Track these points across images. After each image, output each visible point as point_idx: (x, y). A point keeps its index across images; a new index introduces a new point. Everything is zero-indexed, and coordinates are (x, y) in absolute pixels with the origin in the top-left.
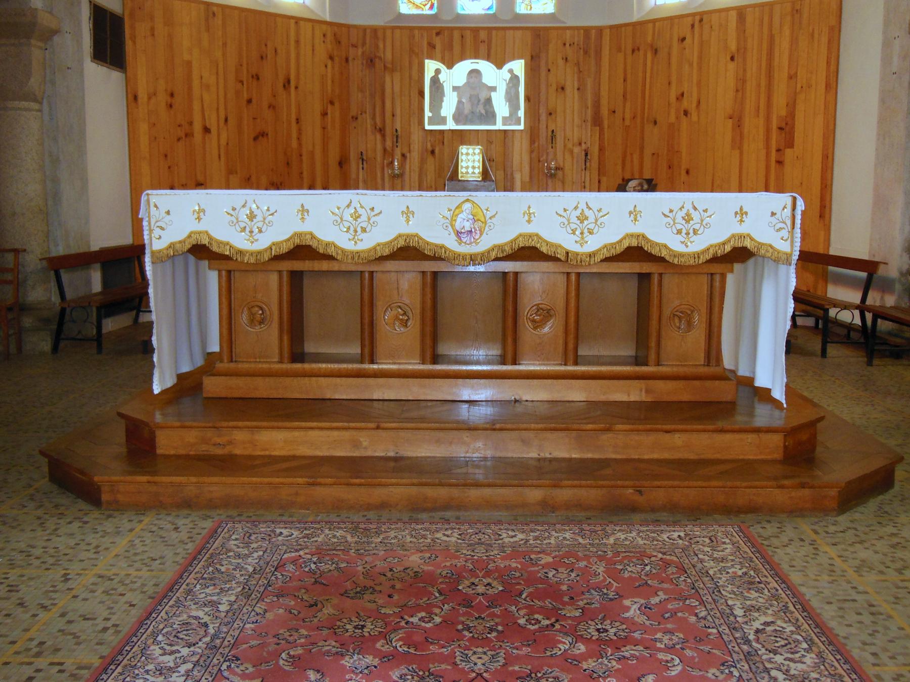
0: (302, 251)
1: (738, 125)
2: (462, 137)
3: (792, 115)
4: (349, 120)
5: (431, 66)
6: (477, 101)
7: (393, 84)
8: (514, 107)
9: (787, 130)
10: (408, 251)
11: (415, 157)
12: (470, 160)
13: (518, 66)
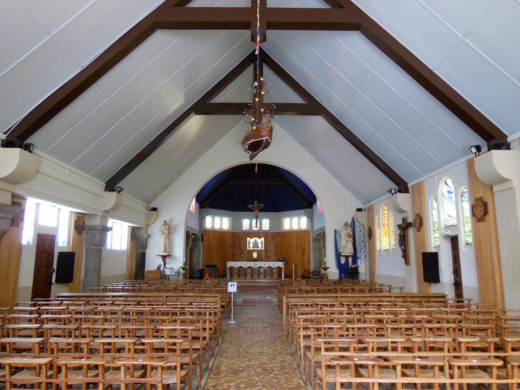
0: (241, 267)
1: (297, 249)
2: (254, 251)
3: (304, 248)
4: (234, 247)
5: (248, 239)
6: (256, 244)
7: (242, 242)
8: (262, 246)
9: (304, 250)
10: (250, 267)
11: (245, 254)
12: (255, 255)
13: (263, 239)
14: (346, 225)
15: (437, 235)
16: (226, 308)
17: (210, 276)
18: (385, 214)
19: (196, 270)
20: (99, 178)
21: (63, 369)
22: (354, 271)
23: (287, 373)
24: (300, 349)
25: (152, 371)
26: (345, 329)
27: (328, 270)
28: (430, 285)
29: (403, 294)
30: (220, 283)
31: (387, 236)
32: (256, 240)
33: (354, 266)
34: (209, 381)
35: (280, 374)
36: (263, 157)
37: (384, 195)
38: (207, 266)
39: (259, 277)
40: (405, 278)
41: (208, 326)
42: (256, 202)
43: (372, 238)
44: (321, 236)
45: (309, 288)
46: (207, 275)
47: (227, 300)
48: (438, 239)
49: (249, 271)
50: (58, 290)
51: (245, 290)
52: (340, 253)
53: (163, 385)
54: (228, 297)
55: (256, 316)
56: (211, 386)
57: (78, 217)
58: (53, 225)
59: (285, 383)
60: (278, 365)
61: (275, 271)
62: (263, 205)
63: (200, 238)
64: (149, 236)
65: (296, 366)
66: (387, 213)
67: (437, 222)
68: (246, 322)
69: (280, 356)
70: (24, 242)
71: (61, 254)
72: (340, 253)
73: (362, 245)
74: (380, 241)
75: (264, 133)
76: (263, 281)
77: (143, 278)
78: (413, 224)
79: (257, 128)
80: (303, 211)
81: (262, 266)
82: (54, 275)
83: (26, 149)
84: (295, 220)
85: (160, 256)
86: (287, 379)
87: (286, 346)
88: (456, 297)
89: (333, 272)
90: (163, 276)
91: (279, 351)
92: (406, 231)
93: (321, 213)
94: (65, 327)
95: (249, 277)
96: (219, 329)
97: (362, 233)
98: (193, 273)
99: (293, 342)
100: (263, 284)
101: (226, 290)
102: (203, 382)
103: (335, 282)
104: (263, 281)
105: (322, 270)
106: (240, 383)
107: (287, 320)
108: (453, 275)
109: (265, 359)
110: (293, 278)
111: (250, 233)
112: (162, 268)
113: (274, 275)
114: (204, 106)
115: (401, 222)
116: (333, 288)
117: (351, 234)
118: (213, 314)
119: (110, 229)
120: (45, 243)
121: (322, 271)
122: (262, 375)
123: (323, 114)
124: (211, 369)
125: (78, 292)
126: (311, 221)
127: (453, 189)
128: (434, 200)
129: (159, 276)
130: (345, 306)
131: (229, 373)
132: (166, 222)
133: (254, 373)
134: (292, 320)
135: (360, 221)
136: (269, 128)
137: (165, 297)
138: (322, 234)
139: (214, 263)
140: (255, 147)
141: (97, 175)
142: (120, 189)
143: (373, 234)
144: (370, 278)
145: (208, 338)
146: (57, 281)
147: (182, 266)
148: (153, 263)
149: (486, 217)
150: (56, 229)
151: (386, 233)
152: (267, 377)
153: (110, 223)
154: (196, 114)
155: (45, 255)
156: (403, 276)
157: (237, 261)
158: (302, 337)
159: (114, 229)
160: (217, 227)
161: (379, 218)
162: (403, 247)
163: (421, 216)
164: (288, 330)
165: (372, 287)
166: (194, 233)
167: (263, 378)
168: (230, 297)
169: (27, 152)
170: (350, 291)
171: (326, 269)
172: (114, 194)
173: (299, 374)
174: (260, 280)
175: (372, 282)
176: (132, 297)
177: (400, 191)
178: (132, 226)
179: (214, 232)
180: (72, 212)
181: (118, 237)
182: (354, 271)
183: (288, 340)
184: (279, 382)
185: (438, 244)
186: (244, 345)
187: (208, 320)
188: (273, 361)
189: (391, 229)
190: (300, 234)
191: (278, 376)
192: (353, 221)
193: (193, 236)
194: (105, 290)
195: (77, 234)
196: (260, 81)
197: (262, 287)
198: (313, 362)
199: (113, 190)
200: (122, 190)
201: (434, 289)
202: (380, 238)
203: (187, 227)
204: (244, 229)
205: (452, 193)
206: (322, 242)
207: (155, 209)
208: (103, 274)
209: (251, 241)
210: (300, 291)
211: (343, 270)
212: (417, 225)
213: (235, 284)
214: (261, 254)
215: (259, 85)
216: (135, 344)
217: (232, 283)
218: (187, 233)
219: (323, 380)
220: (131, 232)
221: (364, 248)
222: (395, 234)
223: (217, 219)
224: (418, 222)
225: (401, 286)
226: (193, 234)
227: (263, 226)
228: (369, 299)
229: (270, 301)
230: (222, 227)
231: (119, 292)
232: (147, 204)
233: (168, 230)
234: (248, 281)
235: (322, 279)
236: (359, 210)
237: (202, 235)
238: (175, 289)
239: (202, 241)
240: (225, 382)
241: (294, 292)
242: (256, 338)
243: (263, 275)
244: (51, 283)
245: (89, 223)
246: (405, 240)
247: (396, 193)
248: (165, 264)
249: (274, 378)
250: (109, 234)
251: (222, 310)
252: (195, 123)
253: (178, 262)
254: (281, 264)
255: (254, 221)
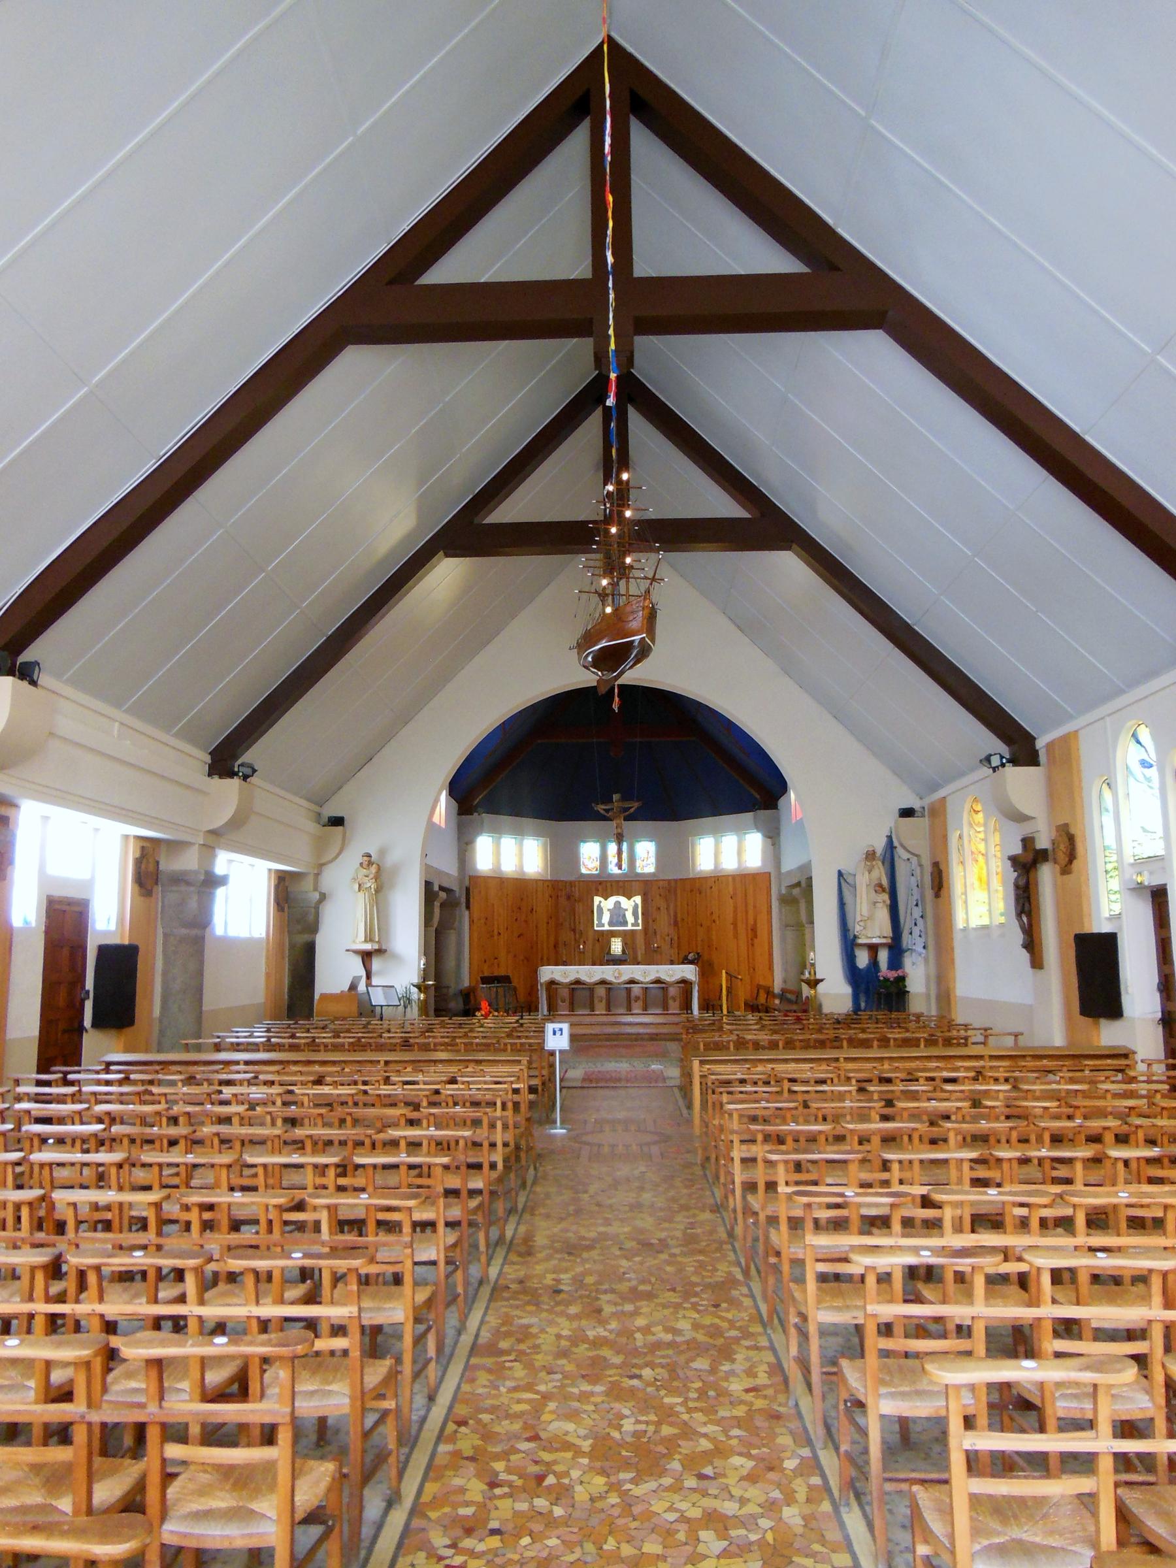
0: (578, 982)
2: (613, 934)
4: (559, 926)
5: (597, 900)
6: (618, 915)
7: (580, 908)
8: (636, 918)
9: (754, 930)
10: (603, 982)
12: (617, 946)
13: (638, 899)
14: (870, 856)
15: (1114, 884)
16: (541, 1098)
17: (494, 1007)
18: (978, 824)
19: (451, 991)
20: (192, 741)
21: (92, 1278)
22: (893, 990)
23: (701, 1252)
24: (733, 1191)
25: (334, 1286)
26: (877, 1164)
27: (820, 987)
28: (1097, 1024)
29: (1023, 1049)
30: (522, 1025)
31: (985, 886)
32: (618, 903)
33: (892, 975)
34: (507, 1269)
35: (684, 1254)
36: (635, 675)
37: (972, 770)
38: (485, 980)
39: (629, 1008)
40: (1031, 1006)
41: (499, 1138)
42: (616, 797)
43: (943, 892)
44: (800, 892)
45: (764, 1037)
46: (484, 1005)
47: (545, 1072)
48: (1118, 896)
49: (601, 991)
50: (97, 1046)
51: (591, 1046)
52: (855, 937)
53: (363, 1327)
54: (545, 1064)
55: (621, 1115)
56: (513, 1281)
57: (143, 848)
58: (86, 876)
59: (696, 1273)
60: (679, 1234)
61: (672, 991)
62: (636, 805)
63: (463, 900)
64: (323, 897)
65: (724, 1236)
66: (982, 821)
67: (1114, 846)
68: (592, 1132)
69: (685, 1213)
70: (17, 921)
71: (103, 950)
72: (855, 937)
73: (917, 913)
74: (966, 902)
75: (634, 625)
76: (639, 1020)
77: (309, 1015)
78: (1050, 853)
79: (616, 610)
80: (750, 815)
81: (638, 977)
82: (89, 1006)
83: (22, 677)
84: (729, 841)
85: (356, 952)
86: (701, 1265)
87: (702, 1189)
88: (1167, 1057)
89: (835, 992)
90: (366, 1010)
91: (682, 1202)
92: (1031, 875)
93: (800, 823)
94: (87, 1158)
95: (600, 1009)
96: (528, 1146)
97: (913, 879)
98: (446, 999)
99: (718, 1178)
100: (642, 1030)
101: (541, 1045)
102: (493, 1272)
103: (839, 1022)
104: (639, 1020)
105: (805, 987)
106: (583, 1274)
107: (706, 1124)
108: (1157, 996)
109: (646, 1222)
110: (725, 1012)
111: (600, 883)
112: (362, 987)
113: (671, 1002)
114: (468, 531)
115: (1017, 849)
116: (833, 1035)
117: (885, 882)
118: (510, 1105)
119: (222, 881)
120: (65, 920)
121: (806, 991)
122: (637, 1255)
123: (794, 546)
124: (511, 1242)
125: (147, 1051)
126: (773, 845)
127: (1152, 757)
128: (1105, 786)
129: (354, 1009)
130: (854, 1082)
131: (557, 1251)
132: (370, 856)
133: (618, 1253)
134: (716, 1122)
135: (909, 843)
136: (646, 611)
137: (382, 1063)
138: (803, 884)
139: (502, 972)
140: (612, 659)
141: (189, 735)
142: (248, 771)
143: (945, 884)
144: (939, 1008)
145: (500, 1166)
146: (95, 1025)
147: (416, 981)
148: (336, 972)
149: (1075, 862)
150: (89, 884)
151: (980, 880)
152: (651, 1262)
153: (225, 862)
154: (447, 556)
155: (66, 952)
156: (1029, 1000)
157: (565, 964)
158: (737, 1162)
159: (231, 880)
160: (509, 867)
161: (960, 837)
162: (1025, 919)
163: (1072, 831)
164: (705, 1149)
165: (946, 1035)
166: (445, 885)
167: (641, 1263)
168: (552, 1066)
169: (25, 684)
170: (875, 1043)
171: (814, 983)
172: (235, 782)
173: (731, 1253)
174: (630, 1019)
175: (946, 1022)
176: (296, 1063)
177: (1015, 761)
178: (278, 871)
179: (500, 882)
180: (127, 837)
181: (242, 905)
182: (893, 990)
183: (705, 1175)
184: (681, 1270)
185: (1117, 908)
186: (592, 1189)
187: (501, 1118)
188: (666, 1225)
189: (994, 869)
190: (747, 884)
191: (679, 1259)
192: (890, 846)
193: (443, 895)
194: (218, 1048)
195: (142, 895)
196: (619, 482)
197: (638, 1037)
198: (762, 1217)
199: (232, 774)
200: (254, 771)
201: (1109, 1035)
202: (965, 893)
203: (427, 868)
204: (584, 871)
205: (1151, 766)
206: (803, 905)
207: (338, 821)
208: (210, 1002)
209: (605, 905)
210: (741, 1044)
211: (863, 986)
212: (1062, 858)
213: (565, 1027)
214: (634, 942)
215: (619, 490)
216: (281, 1209)
217: (557, 1026)
218: (428, 885)
219: (784, 1255)
220: (277, 887)
221: (920, 922)
222: (1004, 883)
223: (508, 843)
224: (1062, 847)
225: (1016, 1030)
226: (442, 888)
227: (638, 863)
228: (917, 1063)
229: (660, 1077)
230: (521, 866)
231: (65, 1102)
232: (317, 809)
233: (377, 877)
234: (597, 1021)
235: (805, 1011)
236: (907, 813)
237: (468, 890)
238: (406, 1044)
239: (468, 907)
240: (547, 1271)
241: (719, 1047)
242: (624, 1170)
243: (640, 1003)
244: (81, 1029)
245: (170, 864)
246: (1029, 898)
247: (1003, 765)
248: (369, 977)
249: (669, 1263)
250: (220, 892)
251: (532, 1097)
252: (446, 575)
253: (404, 972)
254: (689, 972)
255: (612, 848)
